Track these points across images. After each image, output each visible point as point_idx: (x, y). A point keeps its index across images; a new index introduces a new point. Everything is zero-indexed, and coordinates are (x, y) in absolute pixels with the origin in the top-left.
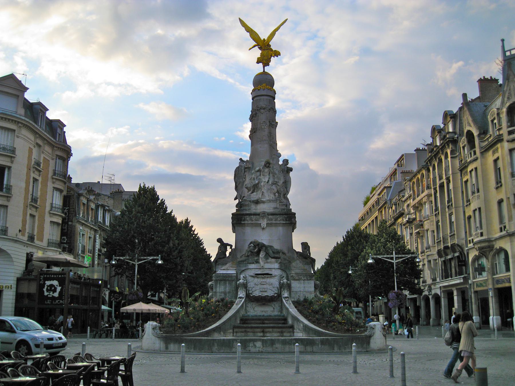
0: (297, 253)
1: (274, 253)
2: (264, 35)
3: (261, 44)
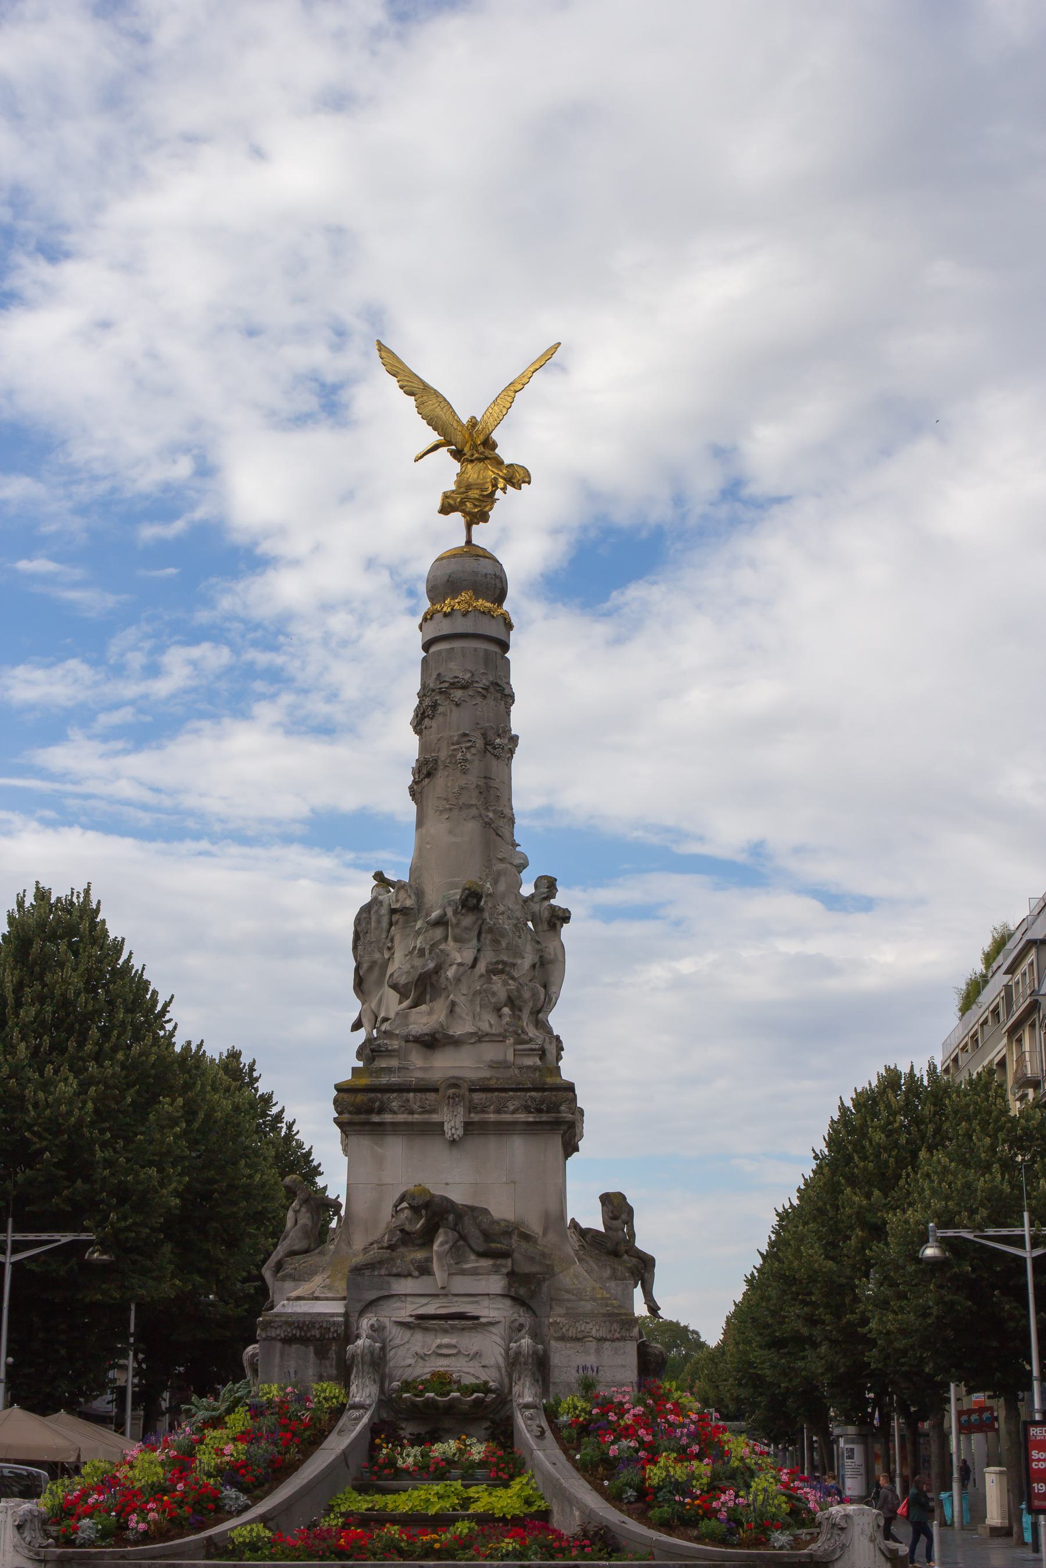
0: (584, 1233)
1: (487, 1236)
2: (467, 407)
3: (459, 438)
